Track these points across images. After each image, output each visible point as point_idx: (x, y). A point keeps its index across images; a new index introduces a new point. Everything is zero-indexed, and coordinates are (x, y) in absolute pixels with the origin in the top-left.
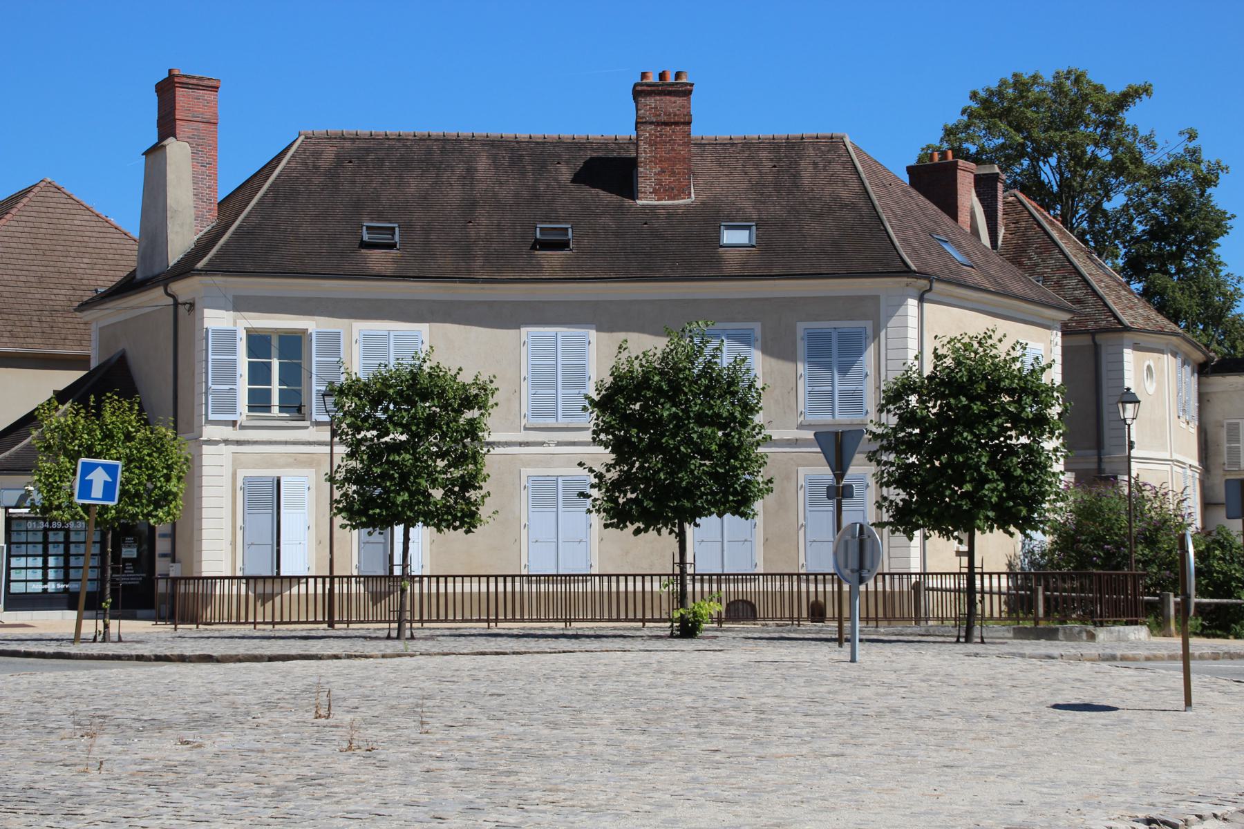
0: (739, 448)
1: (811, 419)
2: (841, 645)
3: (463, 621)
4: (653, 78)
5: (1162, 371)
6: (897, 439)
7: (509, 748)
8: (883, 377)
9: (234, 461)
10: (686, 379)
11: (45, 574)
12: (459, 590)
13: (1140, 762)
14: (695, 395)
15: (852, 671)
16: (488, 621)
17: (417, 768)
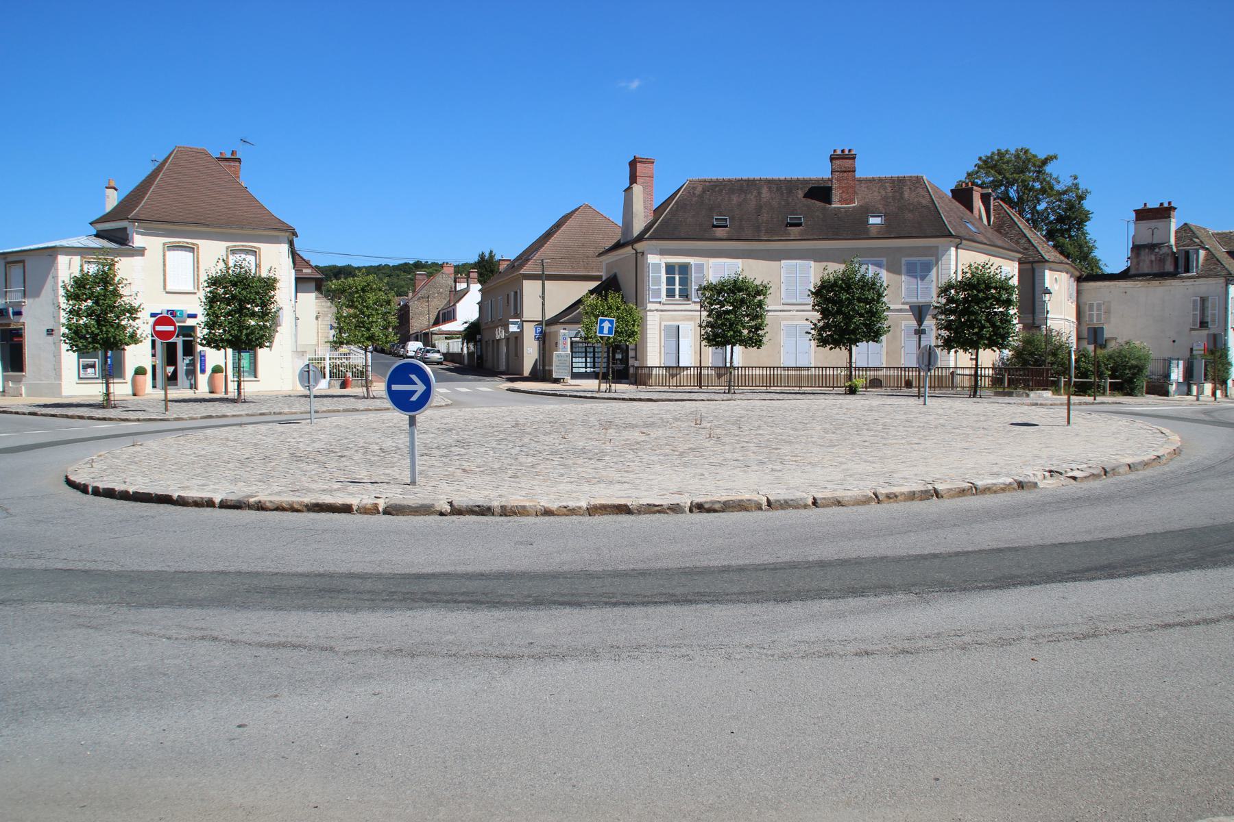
0: (876, 313)
1: (908, 300)
2: (919, 398)
3: (756, 386)
4: (839, 152)
5: (1061, 280)
6: (946, 309)
7: (777, 439)
8: (940, 282)
9: (660, 318)
10: (853, 282)
11: (586, 365)
12: (824, 373)
13: (1047, 447)
14: (857, 289)
15: (924, 409)
16: (766, 386)
17: (738, 446)
